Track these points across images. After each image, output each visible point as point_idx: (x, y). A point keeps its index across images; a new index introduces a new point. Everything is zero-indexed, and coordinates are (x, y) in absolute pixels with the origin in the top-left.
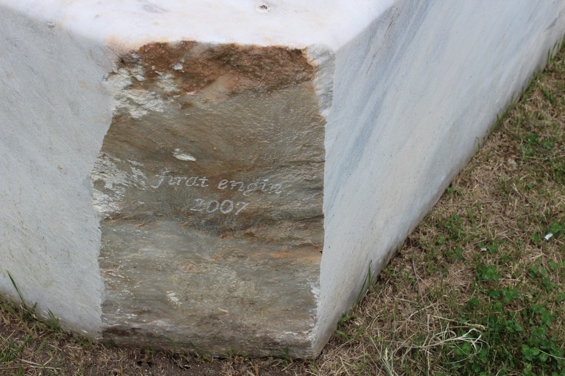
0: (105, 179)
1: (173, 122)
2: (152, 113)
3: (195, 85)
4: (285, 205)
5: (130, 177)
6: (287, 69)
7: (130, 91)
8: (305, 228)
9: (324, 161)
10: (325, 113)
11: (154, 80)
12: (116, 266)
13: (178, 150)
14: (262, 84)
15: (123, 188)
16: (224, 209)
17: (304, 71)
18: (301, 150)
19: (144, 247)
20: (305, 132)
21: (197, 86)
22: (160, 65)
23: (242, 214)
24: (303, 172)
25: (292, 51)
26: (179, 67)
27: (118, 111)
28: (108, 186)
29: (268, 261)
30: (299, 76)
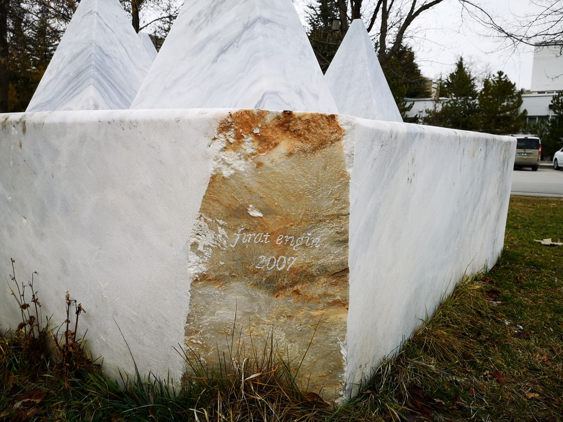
0: (199, 241)
1: (250, 180)
2: (237, 172)
3: (266, 147)
4: (322, 258)
5: (216, 237)
6: (326, 131)
7: (224, 153)
8: (336, 284)
9: (349, 214)
10: (349, 171)
11: (240, 143)
12: (197, 332)
13: (251, 206)
14: (309, 146)
15: (211, 249)
16: (279, 266)
17: (336, 132)
18: (334, 204)
19: (220, 309)
20: (336, 187)
21: (268, 148)
22: (246, 129)
23: (292, 269)
24: (335, 225)
25: (329, 116)
26: (257, 131)
27: (215, 171)
28: (200, 248)
29: (309, 320)
30: (333, 137)
